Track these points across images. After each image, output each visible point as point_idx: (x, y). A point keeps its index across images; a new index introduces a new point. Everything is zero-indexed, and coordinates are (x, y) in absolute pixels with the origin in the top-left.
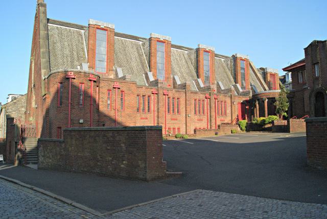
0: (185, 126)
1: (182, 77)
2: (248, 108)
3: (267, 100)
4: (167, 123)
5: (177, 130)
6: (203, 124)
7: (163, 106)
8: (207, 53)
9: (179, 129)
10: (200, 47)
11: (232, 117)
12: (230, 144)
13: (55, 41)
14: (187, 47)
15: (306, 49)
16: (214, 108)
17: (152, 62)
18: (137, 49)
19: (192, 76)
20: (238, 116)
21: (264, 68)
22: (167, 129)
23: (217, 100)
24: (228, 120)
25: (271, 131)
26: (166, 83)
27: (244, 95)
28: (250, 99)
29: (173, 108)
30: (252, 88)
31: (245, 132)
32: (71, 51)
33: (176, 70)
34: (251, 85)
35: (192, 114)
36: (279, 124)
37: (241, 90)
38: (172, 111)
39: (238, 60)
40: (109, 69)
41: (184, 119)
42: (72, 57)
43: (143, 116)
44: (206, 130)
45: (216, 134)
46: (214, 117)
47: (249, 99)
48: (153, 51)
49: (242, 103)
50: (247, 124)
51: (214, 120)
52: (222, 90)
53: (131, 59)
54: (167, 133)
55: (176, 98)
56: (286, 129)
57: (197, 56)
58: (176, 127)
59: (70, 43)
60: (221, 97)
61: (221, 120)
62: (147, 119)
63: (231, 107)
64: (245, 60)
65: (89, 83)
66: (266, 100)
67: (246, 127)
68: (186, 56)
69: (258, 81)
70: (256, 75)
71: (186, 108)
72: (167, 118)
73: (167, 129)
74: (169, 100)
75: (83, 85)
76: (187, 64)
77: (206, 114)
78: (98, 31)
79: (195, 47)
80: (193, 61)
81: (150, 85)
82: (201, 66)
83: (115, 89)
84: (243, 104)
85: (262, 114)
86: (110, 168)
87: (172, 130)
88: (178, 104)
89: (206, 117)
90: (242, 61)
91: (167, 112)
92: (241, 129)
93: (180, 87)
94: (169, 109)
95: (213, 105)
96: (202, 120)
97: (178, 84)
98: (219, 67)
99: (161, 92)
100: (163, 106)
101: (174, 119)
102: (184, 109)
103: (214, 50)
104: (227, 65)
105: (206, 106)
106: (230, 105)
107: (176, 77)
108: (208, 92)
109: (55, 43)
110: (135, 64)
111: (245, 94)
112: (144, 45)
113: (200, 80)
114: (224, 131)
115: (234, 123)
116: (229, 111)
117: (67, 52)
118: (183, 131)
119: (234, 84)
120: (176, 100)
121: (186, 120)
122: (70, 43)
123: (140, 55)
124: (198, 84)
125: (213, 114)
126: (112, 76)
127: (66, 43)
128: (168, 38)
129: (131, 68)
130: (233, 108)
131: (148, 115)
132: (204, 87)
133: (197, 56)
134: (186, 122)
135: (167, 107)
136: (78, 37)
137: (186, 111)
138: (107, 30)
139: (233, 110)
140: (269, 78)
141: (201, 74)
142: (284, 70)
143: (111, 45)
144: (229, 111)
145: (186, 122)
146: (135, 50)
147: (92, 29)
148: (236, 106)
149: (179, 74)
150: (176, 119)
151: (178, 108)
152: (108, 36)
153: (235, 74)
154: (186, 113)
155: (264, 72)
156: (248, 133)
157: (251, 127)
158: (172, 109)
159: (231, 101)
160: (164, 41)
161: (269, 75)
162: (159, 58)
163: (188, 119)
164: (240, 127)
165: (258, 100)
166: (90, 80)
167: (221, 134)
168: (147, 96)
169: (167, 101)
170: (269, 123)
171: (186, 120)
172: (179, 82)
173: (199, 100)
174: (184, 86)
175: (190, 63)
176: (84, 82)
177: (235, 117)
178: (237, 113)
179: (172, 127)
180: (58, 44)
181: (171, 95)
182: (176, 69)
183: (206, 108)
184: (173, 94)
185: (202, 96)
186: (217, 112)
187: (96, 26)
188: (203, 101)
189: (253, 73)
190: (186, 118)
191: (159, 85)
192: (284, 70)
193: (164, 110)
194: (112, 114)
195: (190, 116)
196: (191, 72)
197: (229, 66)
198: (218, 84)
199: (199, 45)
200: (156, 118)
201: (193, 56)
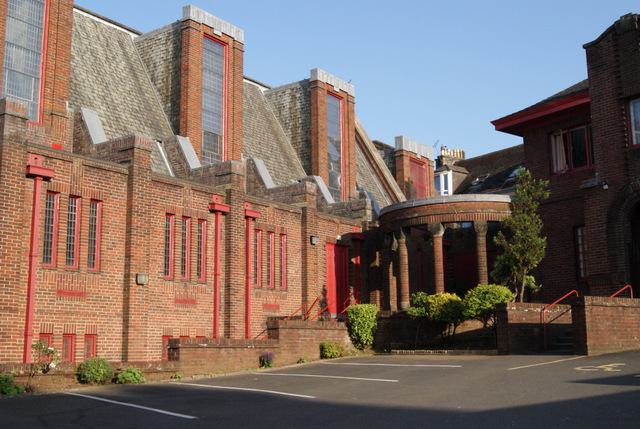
0: (119, 328)
1: (112, 120)
2: (362, 261)
3: (442, 233)
4: (36, 306)
5: (80, 344)
6: (195, 322)
7: (21, 226)
8: (216, 48)
9: (90, 337)
10: (193, 16)
11: (305, 295)
15: (591, 49)
16: (242, 253)
19: (155, 127)
20: (324, 292)
22: (34, 340)
23: (252, 225)
25: (495, 347)
28: (364, 232)
31: (369, 353)
33: (88, 92)
35: (151, 275)
36: (524, 320)
37: (330, 199)
38: (62, 257)
44: (223, 345)
45: (264, 361)
47: (360, 230)
50: (379, 319)
51: (242, 304)
52: (269, 192)
54: (32, 358)
55: (87, 198)
56: (568, 340)
58: (80, 332)
60: (269, 215)
61: (267, 306)
64: (340, 98)
66: (439, 229)
67: (375, 333)
68: (131, 50)
69: (375, 180)
70: (369, 157)
71: (128, 244)
72: (36, 286)
73: (34, 340)
74: (49, 205)
76: (135, 76)
77: (211, 279)
80: (161, 69)
82: (192, 90)
83: (30, 183)
84: (344, 248)
85: (423, 281)
86: (299, 189)
87: (59, 342)
88: (93, 227)
89: (210, 290)
90: (329, 100)
91: (38, 261)
92: (357, 341)
94: (47, 245)
96: (193, 302)
97: (96, 141)
100: (21, 226)
101: (71, 294)
102: (120, 250)
103: (242, 40)
104: (280, 109)
105: (211, 244)
108: (221, 190)
113: (185, 143)
114: (293, 348)
115: (314, 313)
116: (294, 271)
118: (109, 349)
119: (303, 175)
120: (83, 209)
121: (126, 300)
124: (178, 158)
125: (238, 278)
130: (310, 260)
131: (85, 279)
132: (206, 169)
135: (39, 232)
137: (128, 256)
139: (310, 267)
140: (408, 173)
141: (192, 123)
142: (504, 125)
148: (321, 253)
150: (81, 295)
151: (92, 242)
154: (127, 266)
157: (396, 334)
158: (63, 246)
159: (304, 233)
160: (223, 38)
161: (406, 161)
163: (136, 294)
165: (407, 230)
169: (41, 206)
170: (484, 315)
171: (126, 300)
172: (99, 135)
173: (185, 217)
174: (124, 151)
175: (145, 78)
177: (314, 294)
181: (62, 180)
184: (74, 178)
185: (197, 204)
188: (201, 220)
190: (127, 289)
192: (504, 125)
195: (143, 279)
197: (286, 112)
199: (187, 9)
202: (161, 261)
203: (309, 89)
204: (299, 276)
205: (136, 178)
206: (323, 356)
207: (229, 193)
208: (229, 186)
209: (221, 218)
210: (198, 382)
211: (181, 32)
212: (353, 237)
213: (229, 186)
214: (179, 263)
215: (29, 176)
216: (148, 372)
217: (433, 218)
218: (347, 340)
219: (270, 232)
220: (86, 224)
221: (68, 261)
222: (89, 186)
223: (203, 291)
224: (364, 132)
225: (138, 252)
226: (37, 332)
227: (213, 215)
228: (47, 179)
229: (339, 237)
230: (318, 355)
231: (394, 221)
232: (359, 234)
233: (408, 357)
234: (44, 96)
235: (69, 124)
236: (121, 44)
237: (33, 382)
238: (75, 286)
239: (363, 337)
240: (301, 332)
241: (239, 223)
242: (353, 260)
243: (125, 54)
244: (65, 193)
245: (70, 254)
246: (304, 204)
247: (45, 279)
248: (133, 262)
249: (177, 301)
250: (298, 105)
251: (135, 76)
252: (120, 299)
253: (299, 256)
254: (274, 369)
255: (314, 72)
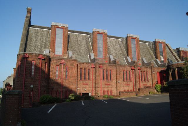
3: (177, 69)
9: (111, 91)
10: (128, 35)
11: (152, 82)
12: (155, 103)
13: (32, 37)
14: (114, 36)
16: (138, 76)
17: (95, 46)
18: (86, 39)
19: (124, 55)
21: (178, 48)
24: (149, 84)
26: (104, 60)
27: (162, 67)
28: (166, 69)
29: (107, 77)
30: (169, 61)
31: (160, 93)
32: (41, 43)
34: (168, 60)
37: (160, 63)
38: (106, 79)
39: (157, 43)
40: (64, 53)
41: (116, 84)
42: (41, 46)
43: (85, 83)
45: (137, 95)
46: (139, 82)
48: (94, 39)
49: (160, 73)
50: (161, 87)
53: (81, 46)
57: (127, 42)
59: (41, 38)
60: (144, 69)
61: (144, 85)
62: (87, 84)
63: (152, 75)
65: (39, 61)
66: (176, 69)
67: (161, 89)
70: (172, 53)
75: (35, 62)
76: (121, 47)
77: (132, 81)
78: (57, 29)
79: (125, 37)
80: (125, 45)
81: (91, 62)
83: (100, 69)
84: (161, 73)
88: (110, 74)
89: (132, 83)
90: (159, 44)
91: (102, 80)
92: (157, 91)
93: (113, 62)
95: (137, 74)
96: (129, 85)
98: (144, 49)
99: (97, 66)
104: (150, 47)
105: (132, 75)
106: (151, 74)
107: (144, 59)
108: (133, 65)
109: (32, 38)
110: (83, 49)
111: (162, 66)
112: (90, 37)
114: (143, 93)
116: (150, 78)
117: (38, 43)
119: (155, 59)
120: (145, 73)
121: (117, 85)
122: (41, 38)
123: (87, 43)
124: (127, 60)
125: (138, 80)
126: (66, 57)
127: (39, 38)
128: (105, 31)
129: (80, 52)
130: (153, 76)
131: (110, 82)
132: (131, 62)
133: (127, 42)
134: (117, 86)
136: (47, 34)
137: (116, 78)
138: (63, 28)
140: (182, 55)
143: (105, 43)
144: (150, 78)
145: (117, 86)
146: (84, 40)
147: (94, 34)
148: (156, 75)
149: (114, 54)
150: (109, 85)
152: (64, 32)
153: (156, 53)
154: (117, 80)
155: (178, 51)
156: (162, 94)
159: (151, 71)
160: (135, 38)
161: (181, 52)
162: (100, 44)
164: (156, 89)
166: (40, 59)
167: (141, 94)
168: (87, 69)
171: (117, 85)
173: (126, 71)
174: (149, 64)
175: (123, 47)
176: (35, 60)
177: (155, 81)
178: (156, 80)
179: (106, 90)
180: (34, 39)
181: (105, 68)
182: (111, 49)
183: (132, 77)
185: (129, 68)
186: (140, 78)
187: (55, 26)
188: (130, 71)
189: (170, 52)
191: (96, 62)
193: (100, 78)
194: (60, 81)
196: (123, 52)
198: (142, 60)
200: (94, 84)
201: (125, 42)
202: (123, 78)
203: (155, 42)
204: (151, 79)
205: (117, 66)
206: (150, 94)
207: (135, 66)
208: (135, 65)
209: (134, 70)
210: (140, 97)
211: (127, 38)
212: (163, 71)
213: (135, 65)
214: (126, 78)
215: (100, 68)
216: (115, 97)
217: (174, 67)
218: (155, 91)
219: (144, 72)
220: (109, 74)
221: (107, 80)
222: (109, 68)
223: (131, 83)
224: (171, 48)
225: (118, 78)
226: (103, 91)
227: (132, 70)
228: (103, 68)
229: (160, 71)
230: (149, 94)
231: (169, 67)
232: (165, 70)
233: (166, 94)
234: (104, 54)
235: (108, 58)
236: (118, 42)
237: (97, 98)
238: (108, 83)
239: (158, 90)
240: (145, 90)
241: (137, 71)
242: (164, 75)
243: (119, 44)
244: (106, 70)
245: (107, 79)
246: (151, 66)
247: (103, 83)
248: (117, 79)
249: (126, 85)
250: (153, 46)
251: (121, 47)
252: (116, 85)
253: (151, 75)
254: (138, 96)
255: (155, 39)
